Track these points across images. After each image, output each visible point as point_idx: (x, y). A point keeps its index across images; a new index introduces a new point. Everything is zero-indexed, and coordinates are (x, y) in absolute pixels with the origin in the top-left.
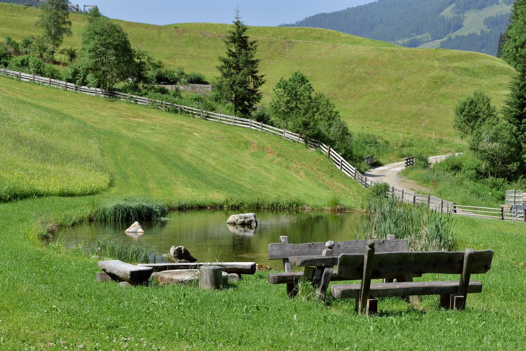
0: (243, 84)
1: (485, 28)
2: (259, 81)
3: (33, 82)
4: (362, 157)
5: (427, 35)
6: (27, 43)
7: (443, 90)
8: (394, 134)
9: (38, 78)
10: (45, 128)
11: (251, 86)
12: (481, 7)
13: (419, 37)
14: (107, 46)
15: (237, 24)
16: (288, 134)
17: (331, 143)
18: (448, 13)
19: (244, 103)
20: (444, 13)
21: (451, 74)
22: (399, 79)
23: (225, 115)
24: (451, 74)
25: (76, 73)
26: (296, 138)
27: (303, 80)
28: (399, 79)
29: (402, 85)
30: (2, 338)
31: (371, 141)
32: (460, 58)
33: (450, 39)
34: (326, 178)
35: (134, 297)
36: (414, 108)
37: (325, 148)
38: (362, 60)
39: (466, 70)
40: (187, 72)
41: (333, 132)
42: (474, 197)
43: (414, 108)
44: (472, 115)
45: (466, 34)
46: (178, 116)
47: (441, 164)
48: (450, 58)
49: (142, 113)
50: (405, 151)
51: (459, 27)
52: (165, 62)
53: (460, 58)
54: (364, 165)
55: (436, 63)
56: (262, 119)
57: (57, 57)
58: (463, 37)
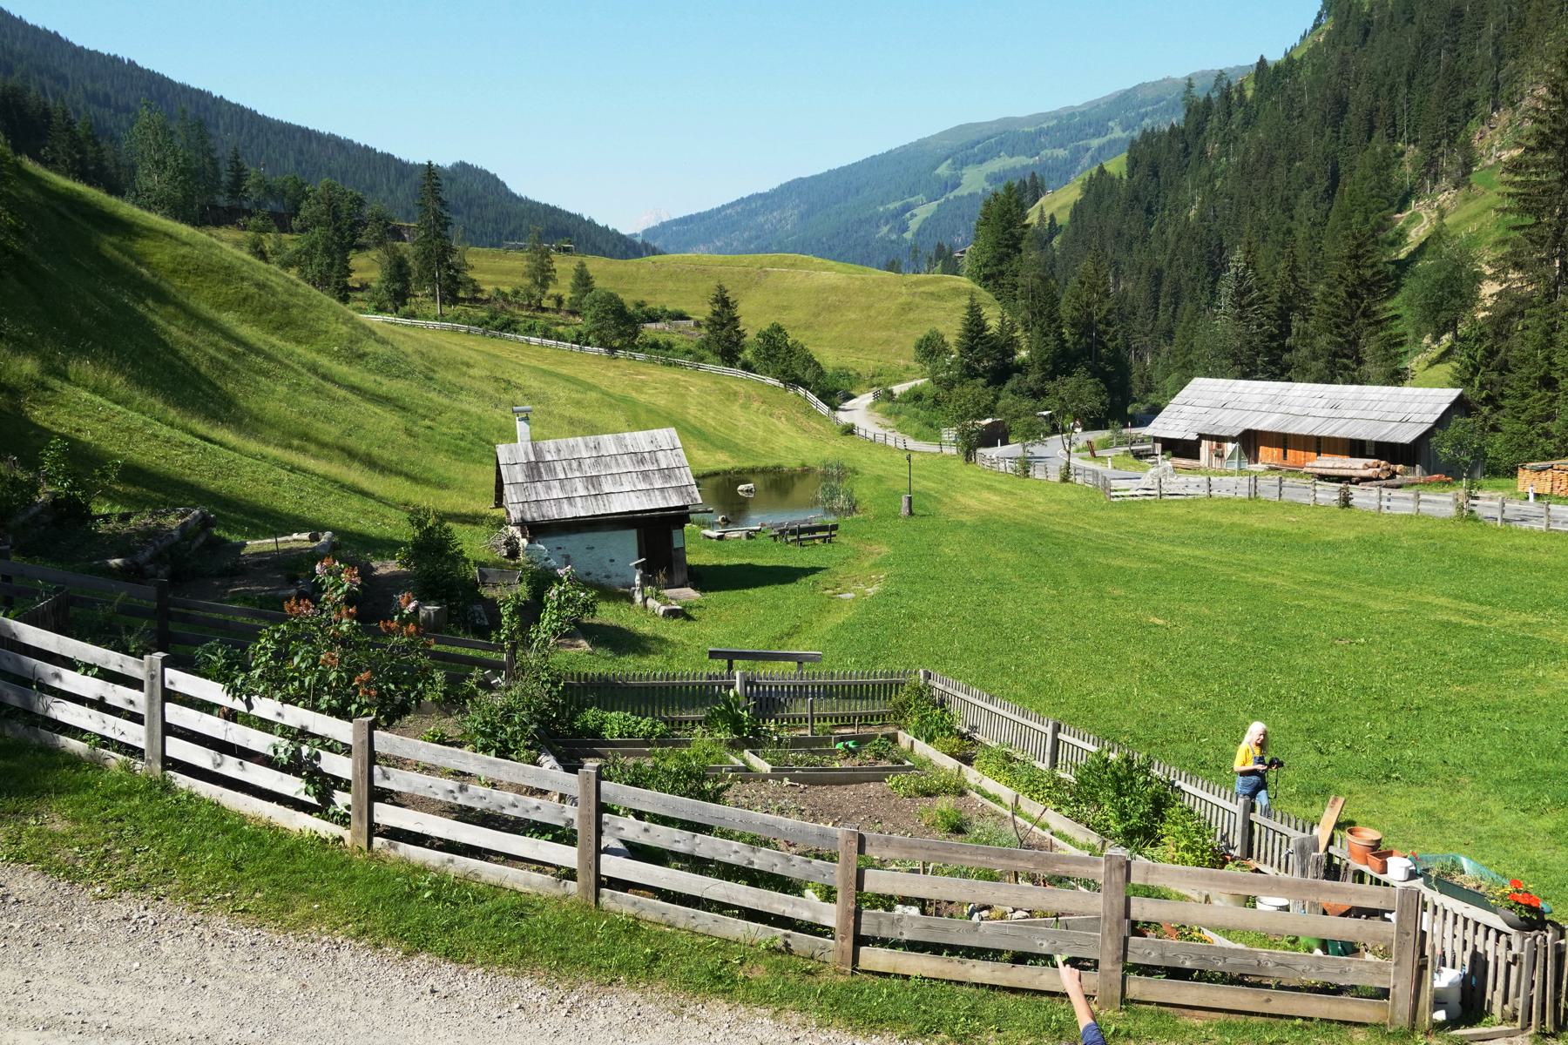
0: (728, 338)
1: (986, 185)
2: (741, 335)
3: (541, 345)
4: (834, 393)
5: (920, 197)
6: (516, 293)
7: (911, 316)
8: (863, 362)
9: (546, 341)
10: (578, 403)
11: (735, 339)
12: (981, 162)
13: (911, 200)
14: (606, 312)
15: (720, 287)
16: (770, 381)
17: (806, 385)
18: (943, 170)
19: (729, 353)
20: (939, 171)
21: (917, 300)
22: (869, 307)
23: (713, 367)
24: (917, 300)
25: (580, 334)
26: (776, 382)
27: (779, 330)
28: (869, 307)
29: (873, 313)
30: (1563, 486)
31: (843, 374)
32: (927, 282)
33: (948, 200)
34: (803, 419)
35: (1233, 640)
36: (885, 334)
37: (801, 391)
38: (834, 289)
39: (932, 294)
40: (669, 309)
41: (808, 375)
42: (926, 430)
43: (885, 334)
44: (930, 349)
45: (966, 193)
46: (673, 369)
47: (904, 395)
48: (917, 284)
49: (642, 370)
50: (875, 381)
51: (957, 185)
52: (646, 298)
53: (927, 282)
54: (837, 400)
55: (904, 290)
56: (747, 367)
57: (545, 303)
58: (963, 197)
